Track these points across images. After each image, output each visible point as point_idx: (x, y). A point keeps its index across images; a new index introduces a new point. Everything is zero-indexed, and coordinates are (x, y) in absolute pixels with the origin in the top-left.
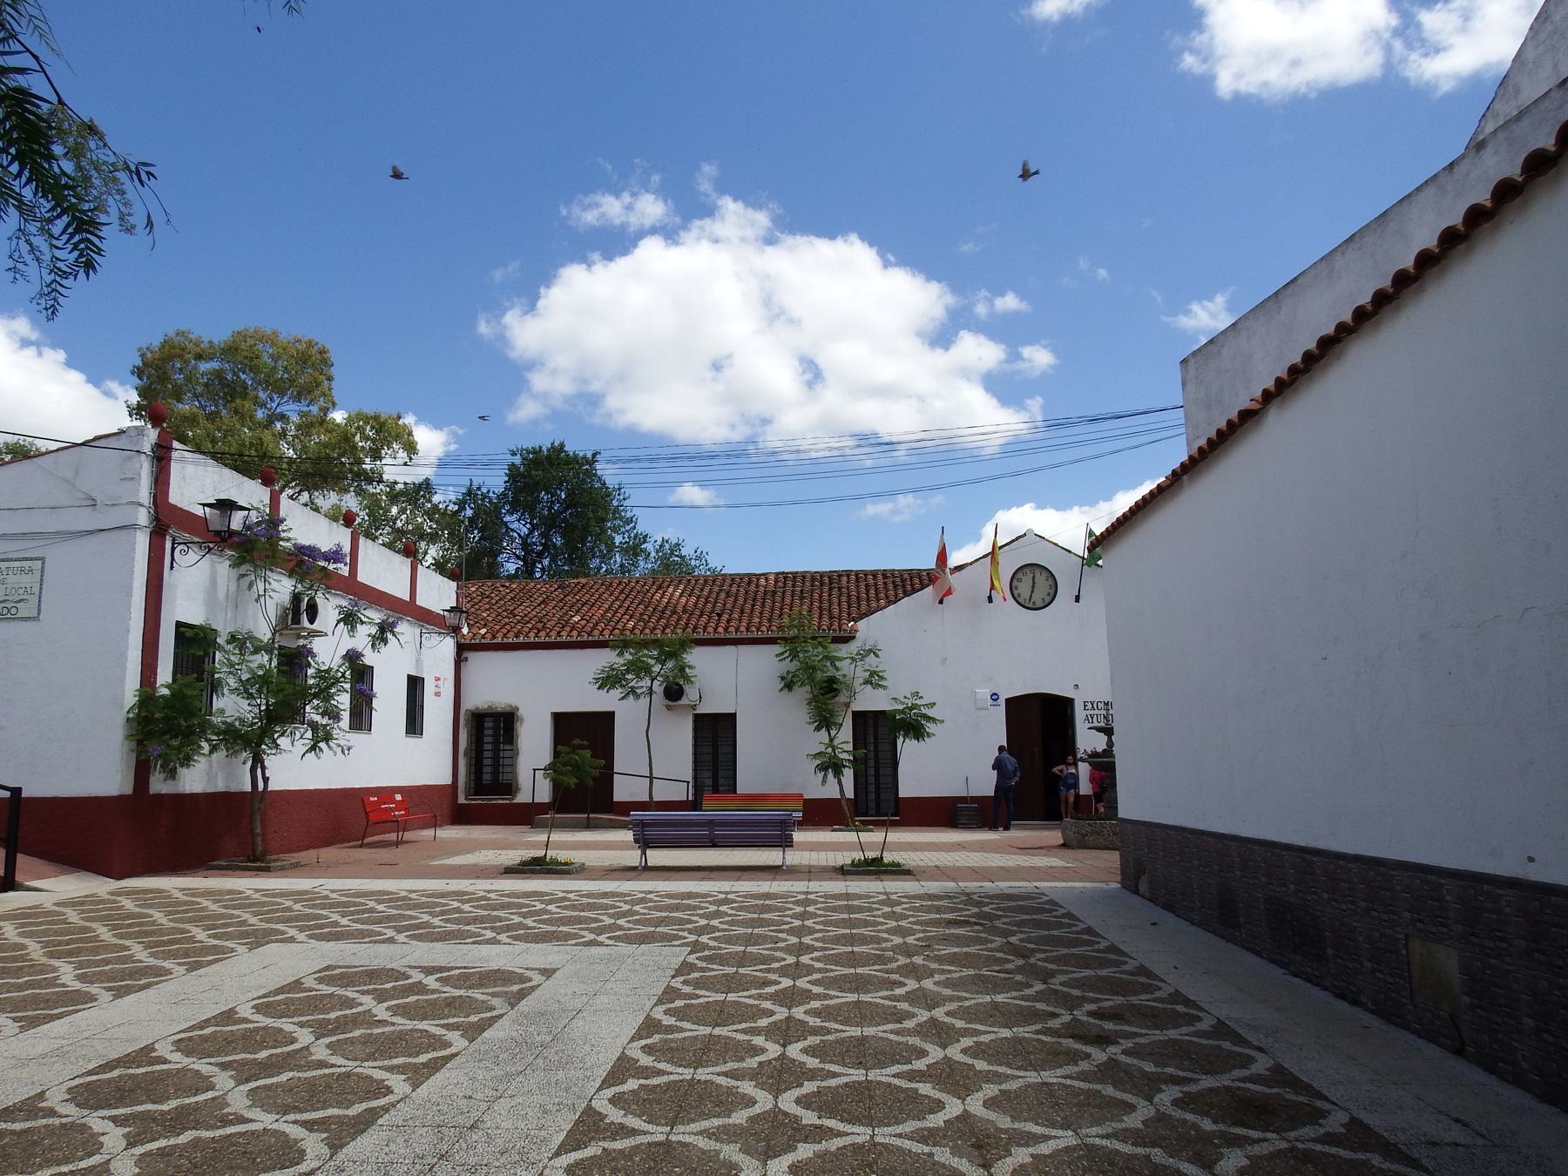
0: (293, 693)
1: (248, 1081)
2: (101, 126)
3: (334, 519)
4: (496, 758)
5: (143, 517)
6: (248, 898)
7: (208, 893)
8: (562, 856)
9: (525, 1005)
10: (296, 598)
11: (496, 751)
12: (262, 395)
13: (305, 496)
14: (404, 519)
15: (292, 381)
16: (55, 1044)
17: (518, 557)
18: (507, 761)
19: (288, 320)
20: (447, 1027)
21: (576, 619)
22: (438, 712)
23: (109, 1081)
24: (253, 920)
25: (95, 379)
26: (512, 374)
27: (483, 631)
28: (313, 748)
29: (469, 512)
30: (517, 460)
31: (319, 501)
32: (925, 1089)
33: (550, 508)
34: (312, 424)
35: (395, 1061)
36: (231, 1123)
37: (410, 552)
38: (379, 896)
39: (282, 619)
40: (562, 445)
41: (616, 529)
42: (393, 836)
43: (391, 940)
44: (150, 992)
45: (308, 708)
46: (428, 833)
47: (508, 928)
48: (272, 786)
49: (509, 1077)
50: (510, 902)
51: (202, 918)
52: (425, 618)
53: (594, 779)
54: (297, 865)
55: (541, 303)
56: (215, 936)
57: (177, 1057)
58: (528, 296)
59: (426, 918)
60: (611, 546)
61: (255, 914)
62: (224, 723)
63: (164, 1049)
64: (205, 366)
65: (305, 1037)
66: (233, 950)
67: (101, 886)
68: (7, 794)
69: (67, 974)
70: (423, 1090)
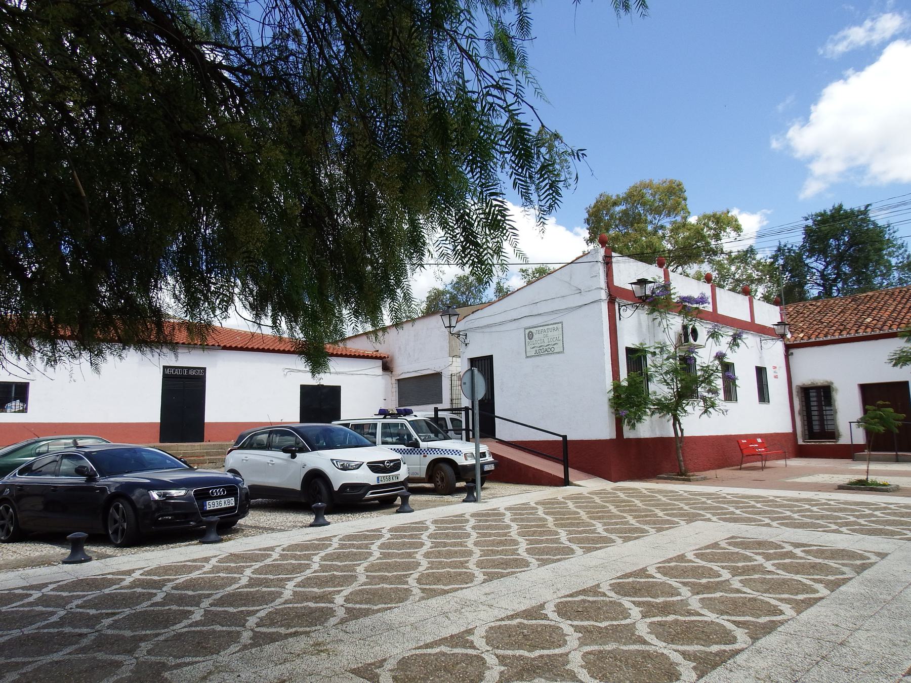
0: (689, 382)
1: (698, 593)
2: (561, 134)
3: (699, 279)
4: (821, 415)
5: (603, 295)
6: (681, 495)
7: (660, 492)
8: (881, 480)
9: (867, 574)
10: (685, 328)
11: (820, 411)
12: (649, 218)
13: (680, 269)
14: (740, 275)
15: (664, 205)
16: (601, 561)
17: (819, 285)
18: (829, 417)
19: (658, 174)
20: (737, 624)
21: (869, 320)
22: (777, 387)
23: (629, 583)
24: (686, 508)
25: (570, 228)
26: (798, 168)
27: (801, 335)
28: (706, 411)
29: (781, 262)
30: (810, 223)
31: (688, 271)
33: (838, 249)
34: (679, 227)
35: (784, 596)
36: (693, 614)
37: (746, 292)
38: (757, 498)
39: (679, 340)
40: (841, 207)
41: (890, 254)
42: (759, 464)
43: (768, 525)
44: (562, 563)
45: (699, 389)
46: (781, 462)
47: (847, 524)
48: (686, 434)
49: (864, 618)
50: (845, 508)
51: (633, 510)
52: (762, 330)
53: (898, 427)
54: (705, 479)
55: (812, 117)
56: (667, 515)
57: (658, 575)
58: (802, 113)
59: (788, 513)
60: (889, 267)
61: (687, 504)
62: (657, 399)
63: (652, 571)
64: (618, 209)
65: (726, 575)
66: (678, 523)
67: (607, 485)
68: (561, 439)
69: (600, 528)
70: (804, 616)
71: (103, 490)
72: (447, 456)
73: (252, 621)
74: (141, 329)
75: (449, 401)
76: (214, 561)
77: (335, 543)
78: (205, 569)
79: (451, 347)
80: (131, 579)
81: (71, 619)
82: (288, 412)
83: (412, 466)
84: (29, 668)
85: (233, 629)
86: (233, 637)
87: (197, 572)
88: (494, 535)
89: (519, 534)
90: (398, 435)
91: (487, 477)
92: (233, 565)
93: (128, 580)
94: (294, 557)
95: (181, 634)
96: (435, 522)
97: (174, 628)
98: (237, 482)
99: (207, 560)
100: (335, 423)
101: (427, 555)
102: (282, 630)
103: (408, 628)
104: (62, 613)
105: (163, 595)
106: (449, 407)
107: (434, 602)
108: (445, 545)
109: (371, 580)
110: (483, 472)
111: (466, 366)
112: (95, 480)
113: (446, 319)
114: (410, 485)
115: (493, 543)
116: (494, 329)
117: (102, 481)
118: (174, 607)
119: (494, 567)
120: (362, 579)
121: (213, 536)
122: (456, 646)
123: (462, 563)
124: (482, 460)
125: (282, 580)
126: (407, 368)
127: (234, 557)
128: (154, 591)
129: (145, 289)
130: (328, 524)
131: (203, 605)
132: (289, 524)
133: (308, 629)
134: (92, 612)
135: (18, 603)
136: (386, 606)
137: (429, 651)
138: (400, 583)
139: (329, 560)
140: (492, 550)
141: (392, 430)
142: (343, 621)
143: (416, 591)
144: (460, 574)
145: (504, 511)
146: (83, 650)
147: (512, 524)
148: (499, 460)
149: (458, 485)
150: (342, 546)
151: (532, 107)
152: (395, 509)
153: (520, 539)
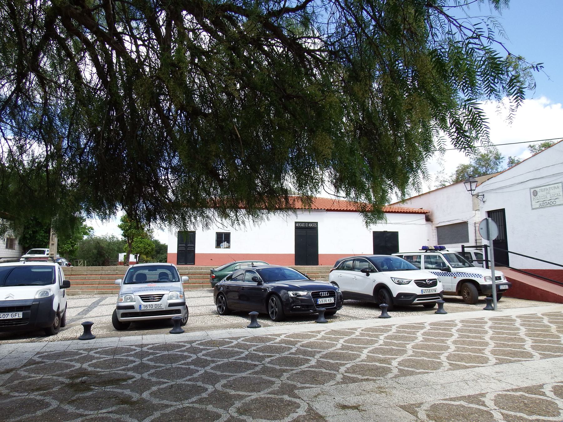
2: (522, 55)
32: (192, 367)
71: (265, 290)
72: (473, 278)
73: (343, 369)
74: (276, 201)
75: (474, 241)
76: (323, 333)
77: (394, 329)
78: (318, 337)
79: (474, 204)
80: (280, 339)
81: (251, 356)
82: (365, 247)
83: (446, 284)
84: (231, 379)
85: (332, 372)
86: (332, 377)
87: (314, 339)
88: (506, 334)
89: (526, 335)
90: (436, 263)
91: (501, 294)
92: (333, 336)
93: (278, 339)
94: (368, 335)
95: (304, 371)
96: (462, 321)
97: (301, 367)
98: (335, 289)
99: (319, 332)
100: (394, 255)
101: (455, 342)
102: (360, 377)
103: (439, 387)
104: (247, 353)
105: (296, 349)
106: (474, 245)
107: (457, 372)
108: (468, 337)
109: (416, 354)
110: (499, 290)
111: (485, 216)
112: (261, 285)
113: (468, 185)
114: (445, 296)
115: (505, 339)
116: (505, 190)
117: (265, 285)
118: (301, 356)
119: (503, 355)
120: (410, 352)
121: (323, 319)
122: (472, 403)
123: (480, 350)
124: (498, 282)
125: (360, 348)
126: (444, 218)
127: (334, 332)
128: (291, 346)
129: (278, 179)
130: (390, 317)
131: (316, 357)
132: (366, 316)
133: (375, 378)
134: (261, 354)
135: (227, 346)
136: (425, 371)
137: (452, 403)
138: (435, 358)
139: (390, 339)
140: (503, 344)
141: (432, 260)
142: (396, 376)
143: (446, 364)
144: (478, 357)
145: (515, 318)
146: (256, 373)
147: (521, 327)
148: (512, 283)
149: (481, 298)
150: (398, 332)
151: (500, 43)
152: (434, 311)
153: (527, 338)
